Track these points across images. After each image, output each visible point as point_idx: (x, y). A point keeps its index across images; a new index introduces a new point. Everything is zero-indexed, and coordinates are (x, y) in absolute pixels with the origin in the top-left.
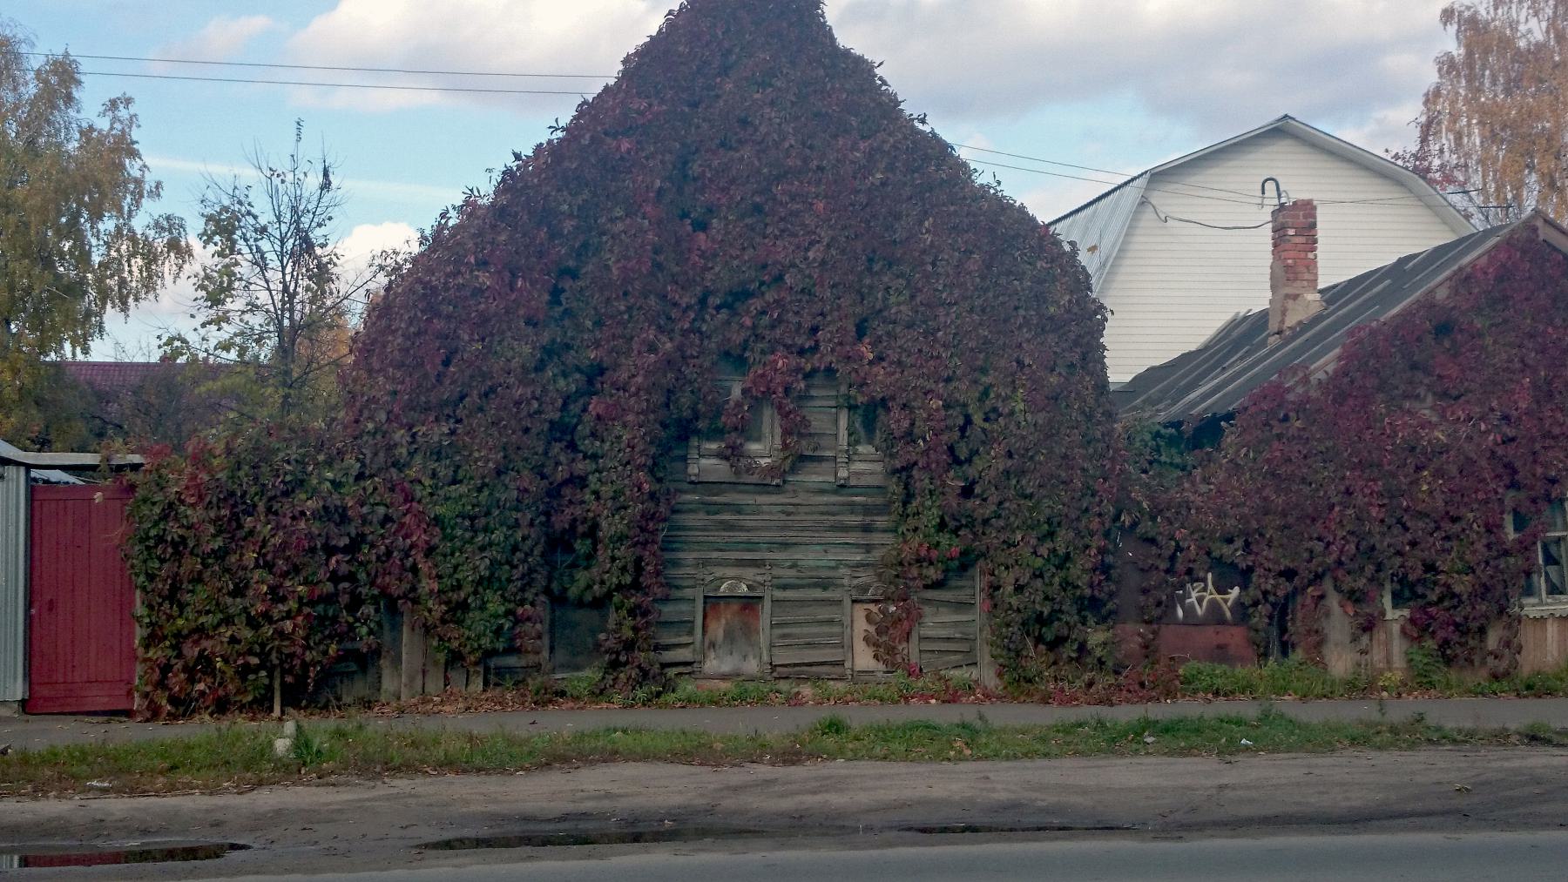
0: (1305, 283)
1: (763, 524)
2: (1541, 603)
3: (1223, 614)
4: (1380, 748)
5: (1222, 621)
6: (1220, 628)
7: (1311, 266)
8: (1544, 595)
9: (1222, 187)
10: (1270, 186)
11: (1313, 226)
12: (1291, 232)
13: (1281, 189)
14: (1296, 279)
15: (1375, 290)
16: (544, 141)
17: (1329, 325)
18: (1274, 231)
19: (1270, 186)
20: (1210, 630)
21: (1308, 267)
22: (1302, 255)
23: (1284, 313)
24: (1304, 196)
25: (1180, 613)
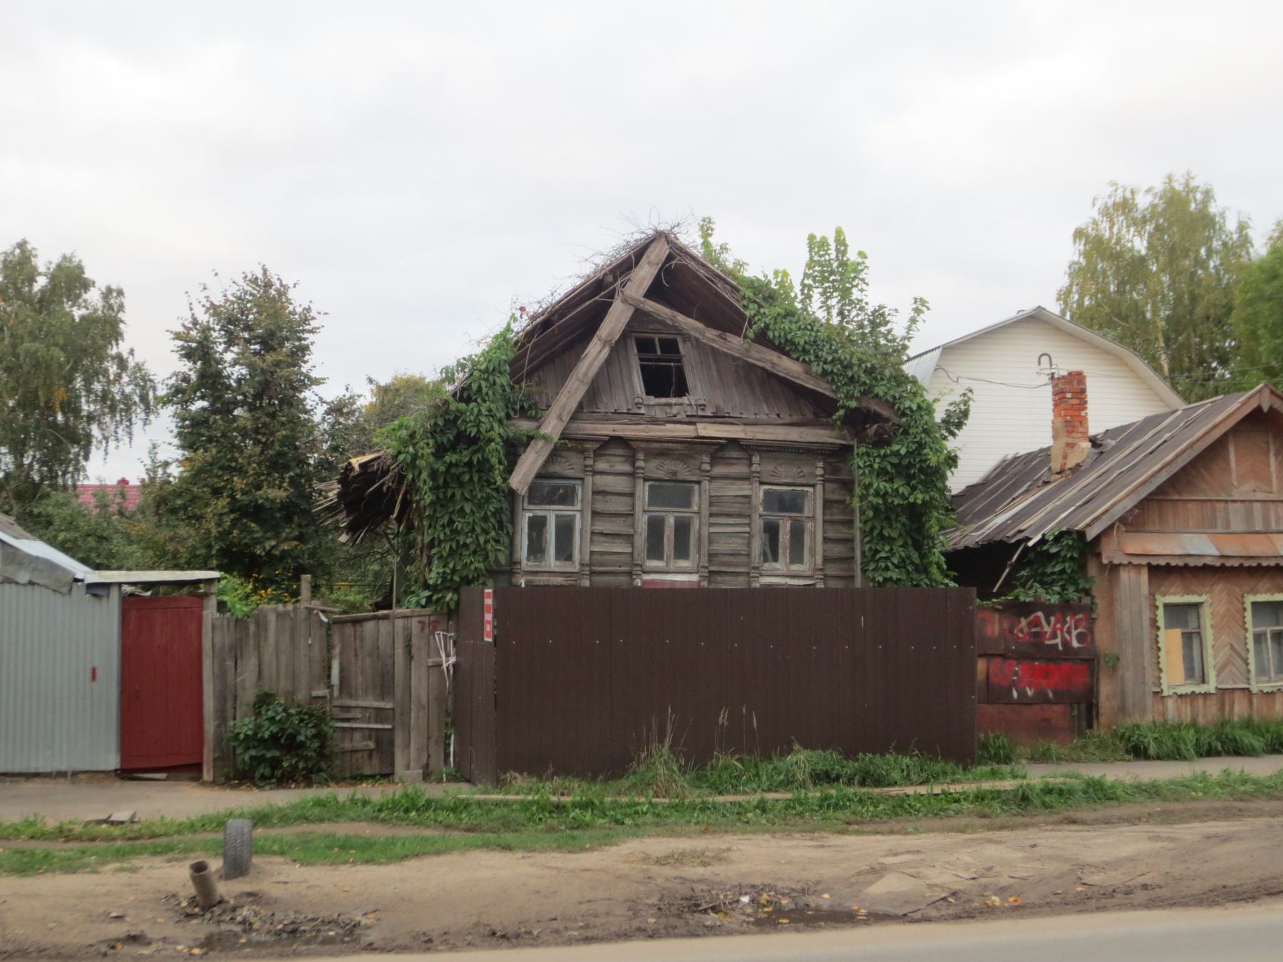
0: (1080, 435)
1: (731, 521)
2: (1269, 681)
3: (1047, 694)
4: (353, 820)
5: (1047, 701)
6: (1046, 706)
7: (1083, 421)
8: (1272, 674)
9: (972, 376)
10: (1045, 359)
11: (1083, 391)
12: (1069, 395)
13: (1054, 362)
14: (1073, 432)
15: (1150, 434)
16: (314, 364)
17: (1217, 415)
18: (1055, 394)
19: (1045, 359)
20: (1037, 708)
21: (1081, 423)
22: (1077, 413)
23: (1065, 457)
24: (1075, 368)
25: (1015, 694)
